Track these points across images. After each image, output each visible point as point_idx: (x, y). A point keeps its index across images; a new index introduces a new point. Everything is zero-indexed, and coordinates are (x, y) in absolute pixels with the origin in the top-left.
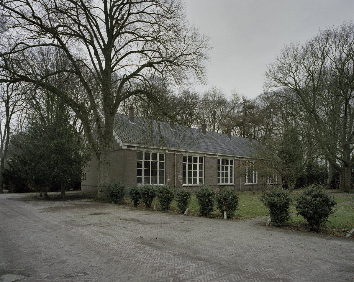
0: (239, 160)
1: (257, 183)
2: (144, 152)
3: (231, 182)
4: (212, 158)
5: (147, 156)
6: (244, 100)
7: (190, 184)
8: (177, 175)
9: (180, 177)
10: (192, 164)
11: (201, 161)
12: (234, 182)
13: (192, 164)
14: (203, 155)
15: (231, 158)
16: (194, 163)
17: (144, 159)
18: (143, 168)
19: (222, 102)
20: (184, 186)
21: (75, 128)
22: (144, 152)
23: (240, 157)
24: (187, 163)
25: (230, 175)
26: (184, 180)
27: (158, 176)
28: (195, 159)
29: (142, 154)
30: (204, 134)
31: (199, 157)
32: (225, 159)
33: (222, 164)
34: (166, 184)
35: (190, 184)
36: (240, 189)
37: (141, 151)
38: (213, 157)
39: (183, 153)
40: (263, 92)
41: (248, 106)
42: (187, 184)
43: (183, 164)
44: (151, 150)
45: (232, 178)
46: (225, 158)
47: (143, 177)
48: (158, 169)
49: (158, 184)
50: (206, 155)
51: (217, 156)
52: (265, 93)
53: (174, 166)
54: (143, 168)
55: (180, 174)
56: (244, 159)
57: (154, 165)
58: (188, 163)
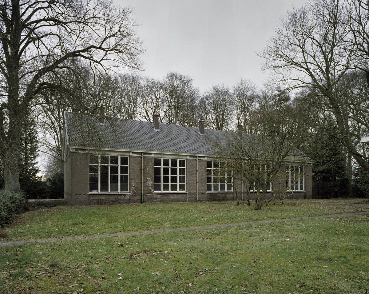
0: (141, 157)
1: (304, 190)
3: (301, 188)
4: (197, 161)
5: (166, 163)
8: (145, 181)
9: (150, 184)
11: (182, 163)
12: (305, 188)
14: (185, 157)
16: (171, 166)
18: (162, 175)
20: (155, 193)
23: (197, 156)
25: (302, 181)
26: (157, 187)
27: (162, 183)
29: (117, 157)
30: (201, 133)
31: (178, 159)
32: (109, 157)
33: (163, 166)
34: (130, 191)
36: (241, 197)
37: (97, 154)
38: (199, 159)
39: (153, 155)
42: (162, 191)
43: (155, 168)
45: (211, 185)
46: (170, 158)
47: (162, 183)
48: (178, 175)
49: (99, 191)
50: (188, 157)
51: (206, 158)
53: (141, 171)
54: (162, 175)
57: (174, 171)
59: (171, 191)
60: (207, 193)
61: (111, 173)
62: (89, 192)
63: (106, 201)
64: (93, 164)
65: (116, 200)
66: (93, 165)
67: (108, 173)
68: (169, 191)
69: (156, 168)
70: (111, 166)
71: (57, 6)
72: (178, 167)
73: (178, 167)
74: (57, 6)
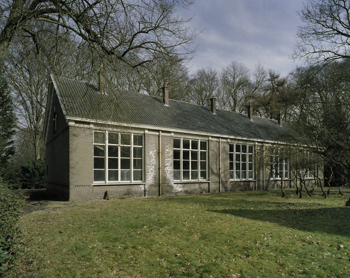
2: (235, 144)
6: (271, 76)
7: (186, 181)
10: (188, 152)
13: (188, 152)
15: (250, 143)
16: (192, 149)
17: (133, 143)
19: (244, 83)
21: (322, 155)
22: (235, 144)
24: (182, 149)
28: (195, 145)
35: (186, 181)
40: (295, 69)
41: (277, 84)
44: (248, 143)
52: (298, 69)
55: (168, 166)
56: (172, 134)
57: (194, 155)
58: (200, 151)
59: (192, 179)
60: (230, 182)
61: (118, 159)
62: (94, 182)
63: (116, 194)
64: (99, 144)
65: (128, 192)
66: (99, 145)
67: (129, 156)
68: (189, 179)
69: (111, 146)
70: (191, 151)
71: (94, 12)
72: (199, 160)
73: (199, 160)
74: (94, 12)
